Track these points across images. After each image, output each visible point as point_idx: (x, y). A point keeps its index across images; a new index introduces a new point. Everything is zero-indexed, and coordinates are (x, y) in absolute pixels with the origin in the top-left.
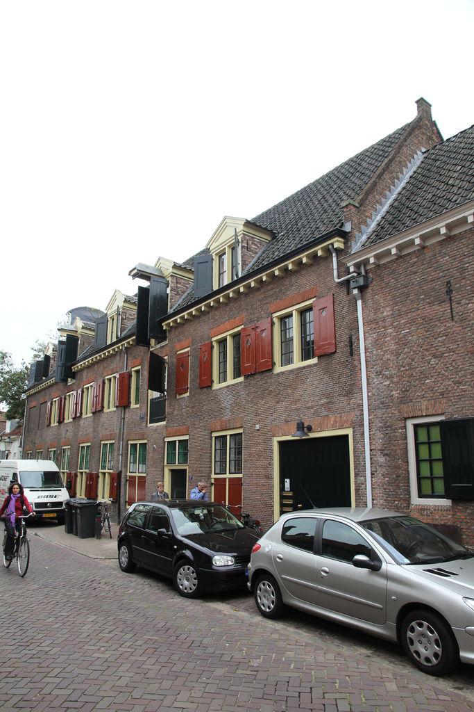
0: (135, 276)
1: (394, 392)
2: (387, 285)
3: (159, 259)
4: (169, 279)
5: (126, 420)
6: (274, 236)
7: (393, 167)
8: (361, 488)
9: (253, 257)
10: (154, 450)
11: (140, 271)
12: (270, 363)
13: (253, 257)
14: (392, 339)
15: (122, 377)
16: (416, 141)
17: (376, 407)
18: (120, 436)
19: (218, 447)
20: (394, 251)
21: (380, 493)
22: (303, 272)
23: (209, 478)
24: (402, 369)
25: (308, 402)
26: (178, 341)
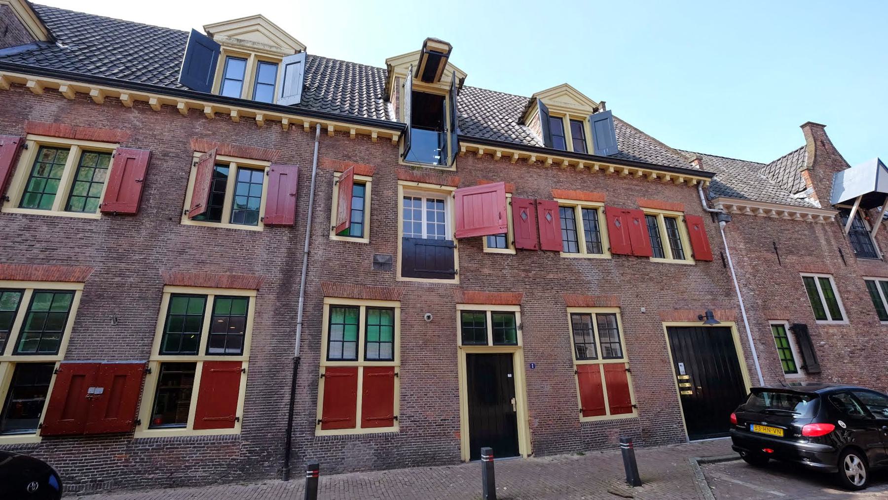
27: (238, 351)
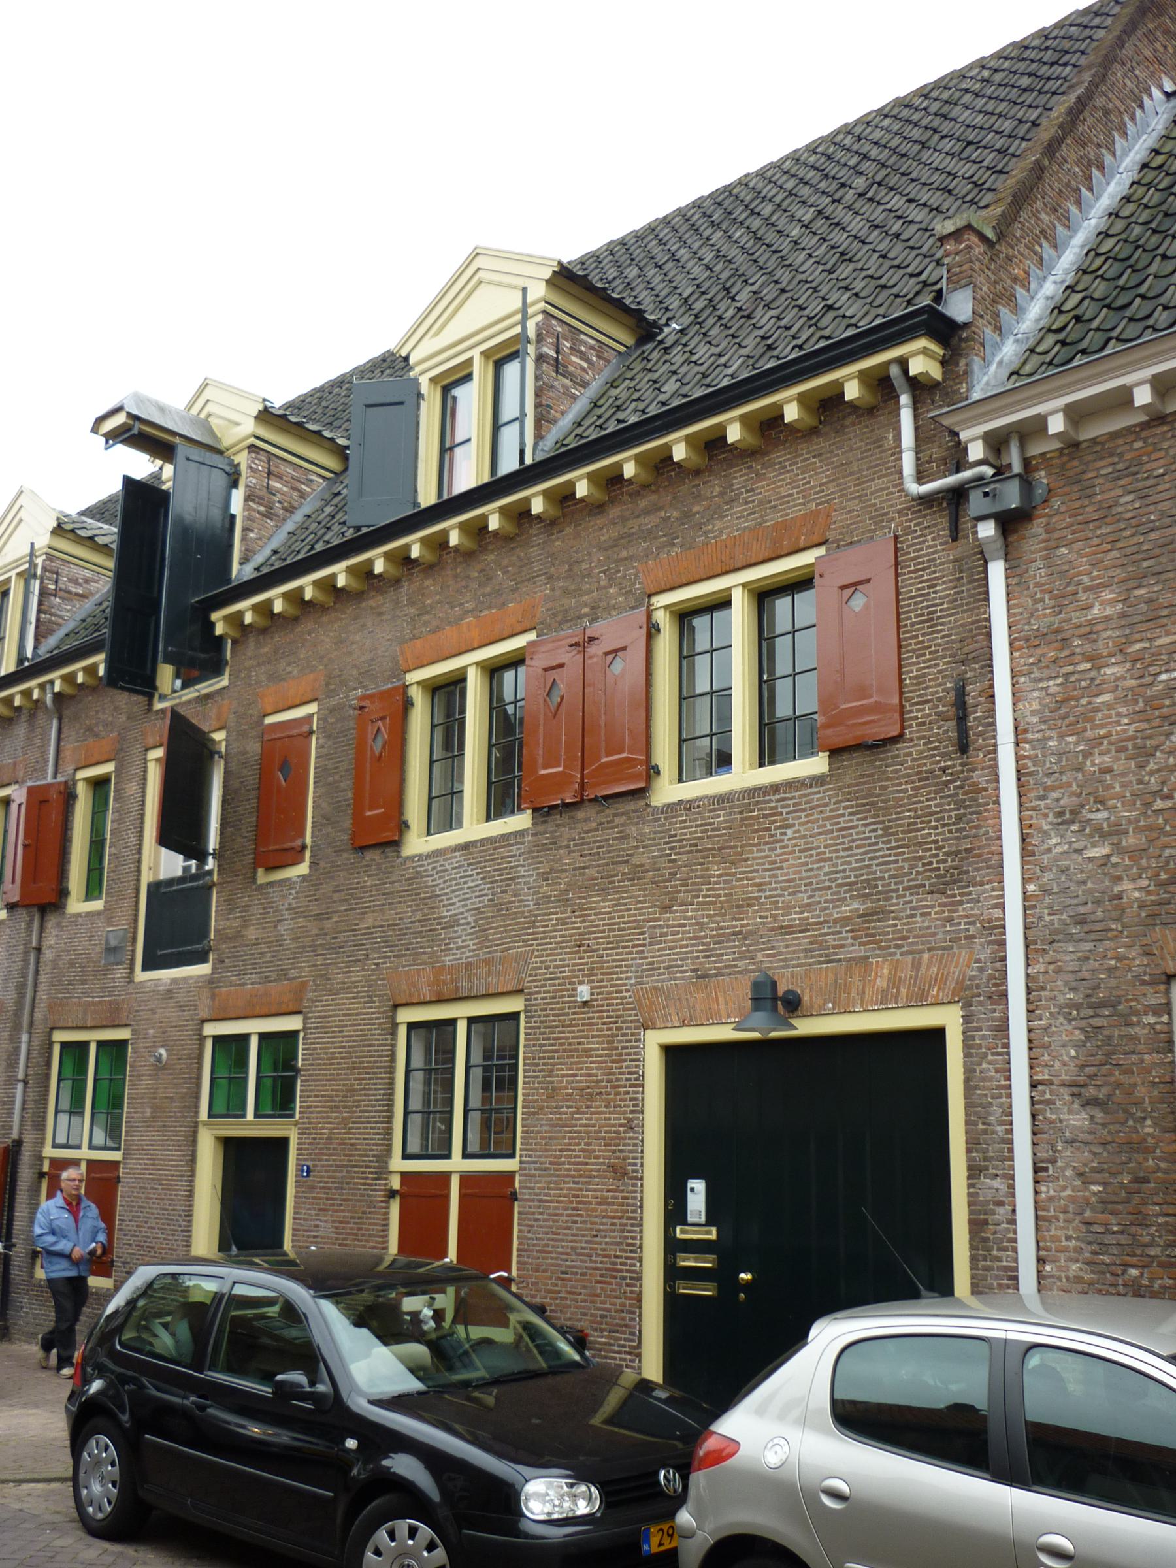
0: (114, 437)
1: (1127, 885)
2: (1106, 514)
3: (205, 386)
4: (243, 459)
5: (48, 955)
6: (646, 332)
7: (1088, 124)
8: (991, 1218)
9: (574, 398)
10: (159, 1067)
11: (136, 418)
12: (641, 768)
13: (574, 398)
14: (1124, 701)
15: (38, 800)
16: (1147, 53)
17: (1057, 932)
18: (18, 1014)
19: (418, 1061)
20: (1143, 396)
21: (1068, 1238)
22: (780, 456)
23: (383, 1172)
24: (1159, 804)
25: (788, 909)
26: (274, 678)
27: (471, 1149)
